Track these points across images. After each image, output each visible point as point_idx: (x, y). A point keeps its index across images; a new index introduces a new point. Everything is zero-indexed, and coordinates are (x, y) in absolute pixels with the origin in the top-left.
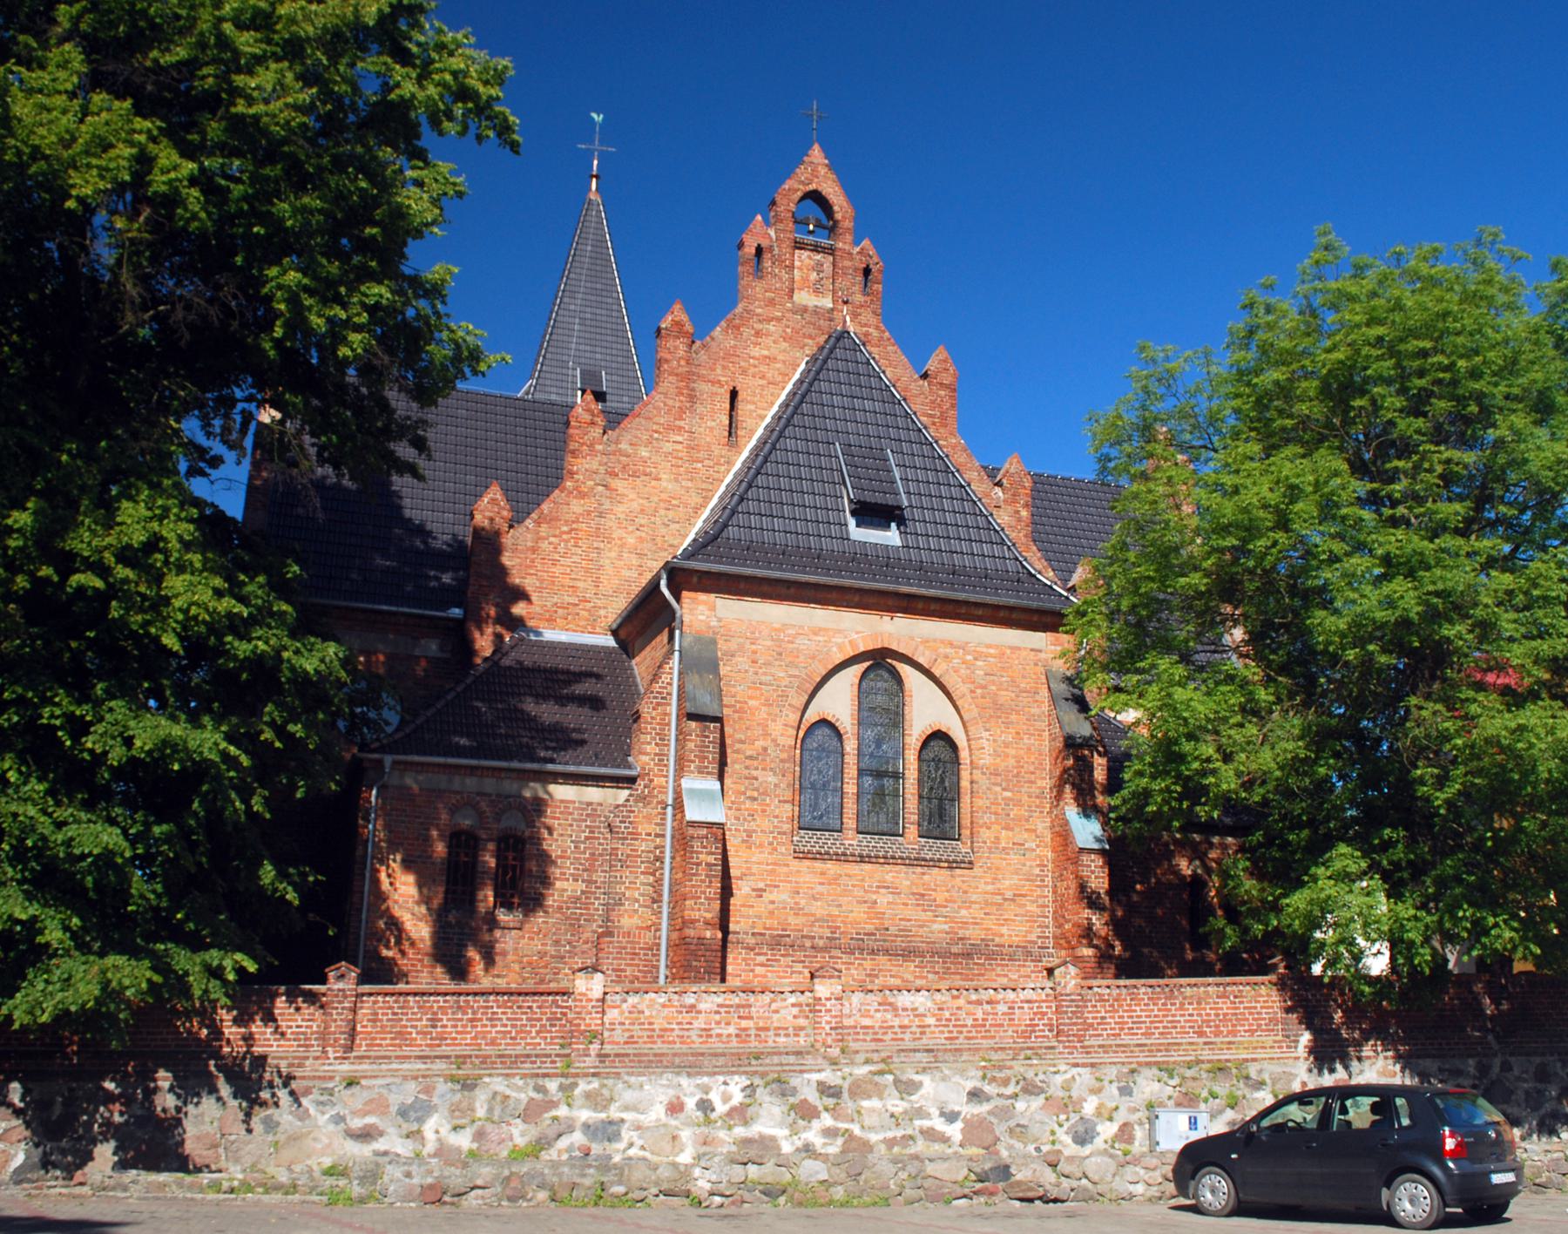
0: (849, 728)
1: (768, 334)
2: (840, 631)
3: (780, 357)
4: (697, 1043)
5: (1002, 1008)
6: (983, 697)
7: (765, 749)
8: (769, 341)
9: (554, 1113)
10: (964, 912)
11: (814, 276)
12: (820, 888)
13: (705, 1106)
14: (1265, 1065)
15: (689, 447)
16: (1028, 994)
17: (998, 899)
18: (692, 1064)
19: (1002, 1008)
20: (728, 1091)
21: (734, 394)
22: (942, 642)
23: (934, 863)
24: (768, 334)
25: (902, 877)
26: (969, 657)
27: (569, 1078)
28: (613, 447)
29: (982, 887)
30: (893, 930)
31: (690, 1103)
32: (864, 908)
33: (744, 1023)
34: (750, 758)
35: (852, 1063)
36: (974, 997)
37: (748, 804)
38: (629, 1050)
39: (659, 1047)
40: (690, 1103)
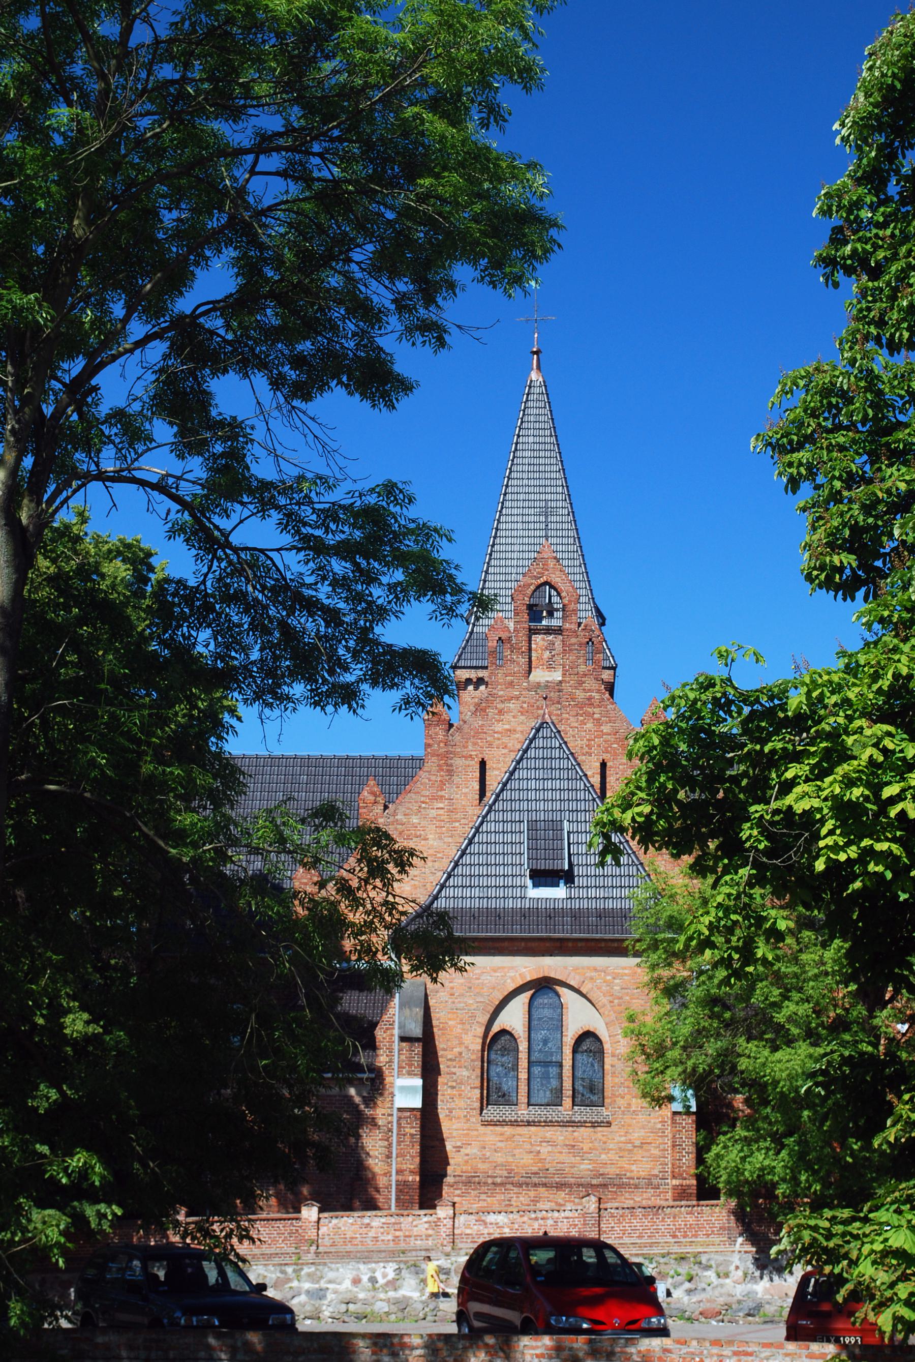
0: (521, 1034)
1: (509, 711)
2: (512, 968)
3: (519, 729)
4: (371, 1245)
5: (550, 1222)
6: (619, 1005)
7: (460, 1054)
8: (506, 717)
9: (290, 1285)
10: (603, 1156)
11: (547, 654)
12: (500, 1144)
13: (373, 1280)
14: (712, 1256)
15: (450, 811)
16: (567, 1214)
17: (630, 1146)
18: (366, 1257)
19: (550, 1222)
20: (386, 1271)
21: (483, 764)
22: (588, 968)
23: (581, 1124)
24: (509, 711)
25: (559, 1135)
26: (609, 978)
27: (299, 1265)
28: (392, 819)
29: (617, 1139)
30: (551, 1170)
31: (365, 1278)
32: (531, 1156)
33: (397, 1233)
34: (450, 1060)
35: (458, 1255)
36: (533, 1216)
37: (449, 1091)
38: (333, 1249)
39: (349, 1248)
40: (365, 1278)
